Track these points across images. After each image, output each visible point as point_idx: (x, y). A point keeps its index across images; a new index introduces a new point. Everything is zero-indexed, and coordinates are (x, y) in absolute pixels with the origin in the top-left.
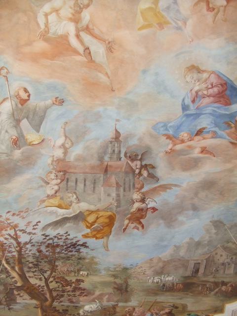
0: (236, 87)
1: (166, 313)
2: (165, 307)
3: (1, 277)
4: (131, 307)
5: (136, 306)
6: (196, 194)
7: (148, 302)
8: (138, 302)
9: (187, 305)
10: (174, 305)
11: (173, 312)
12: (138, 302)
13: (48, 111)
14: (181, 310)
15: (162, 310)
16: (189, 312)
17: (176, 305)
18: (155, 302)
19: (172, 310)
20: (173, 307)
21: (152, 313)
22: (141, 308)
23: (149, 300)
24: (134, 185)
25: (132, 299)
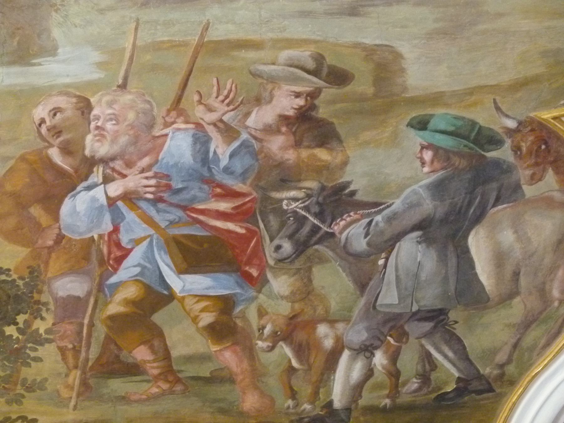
0: (493, 412)
1: (284, 119)
2: (273, 80)
3: (15, 347)
4: (64, 91)
5: (96, 86)
6: (477, 144)
7: (157, 47)
8: (96, 56)
9: (398, 56)
10: (319, 59)
11: (322, 112)
12: (96, 56)
13: (209, 122)
14: (370, 90)
15: (258, 101)
16: (414, 102)
17: (330, 60)
18: (200, 46)
19: (313, 95)
20: (315, 73)
21: (199, 126)
22: (127, 98)
23: (162, 36)
24: (382, 333)
25: (56, 33)
